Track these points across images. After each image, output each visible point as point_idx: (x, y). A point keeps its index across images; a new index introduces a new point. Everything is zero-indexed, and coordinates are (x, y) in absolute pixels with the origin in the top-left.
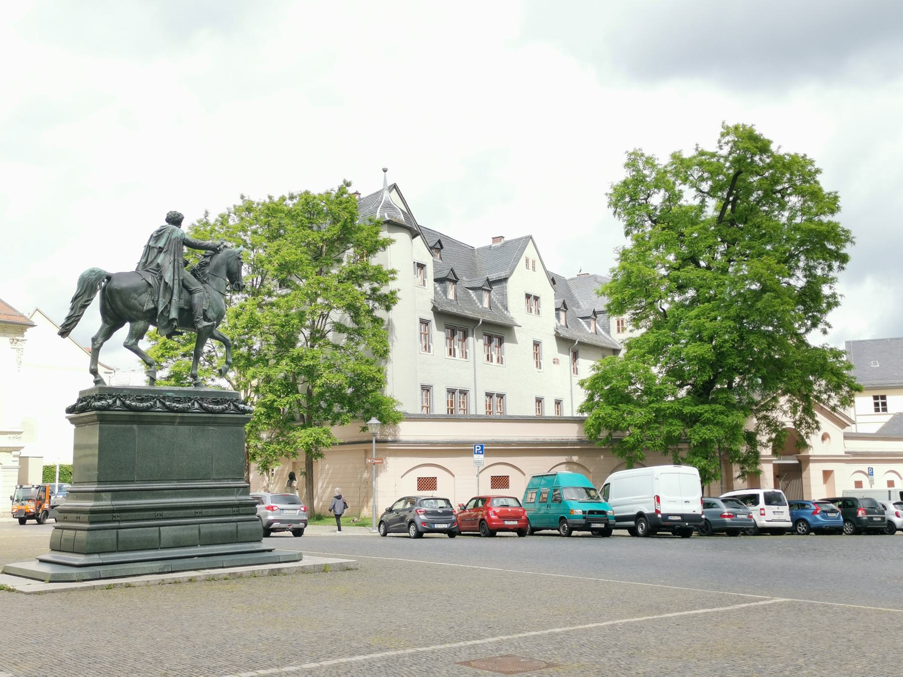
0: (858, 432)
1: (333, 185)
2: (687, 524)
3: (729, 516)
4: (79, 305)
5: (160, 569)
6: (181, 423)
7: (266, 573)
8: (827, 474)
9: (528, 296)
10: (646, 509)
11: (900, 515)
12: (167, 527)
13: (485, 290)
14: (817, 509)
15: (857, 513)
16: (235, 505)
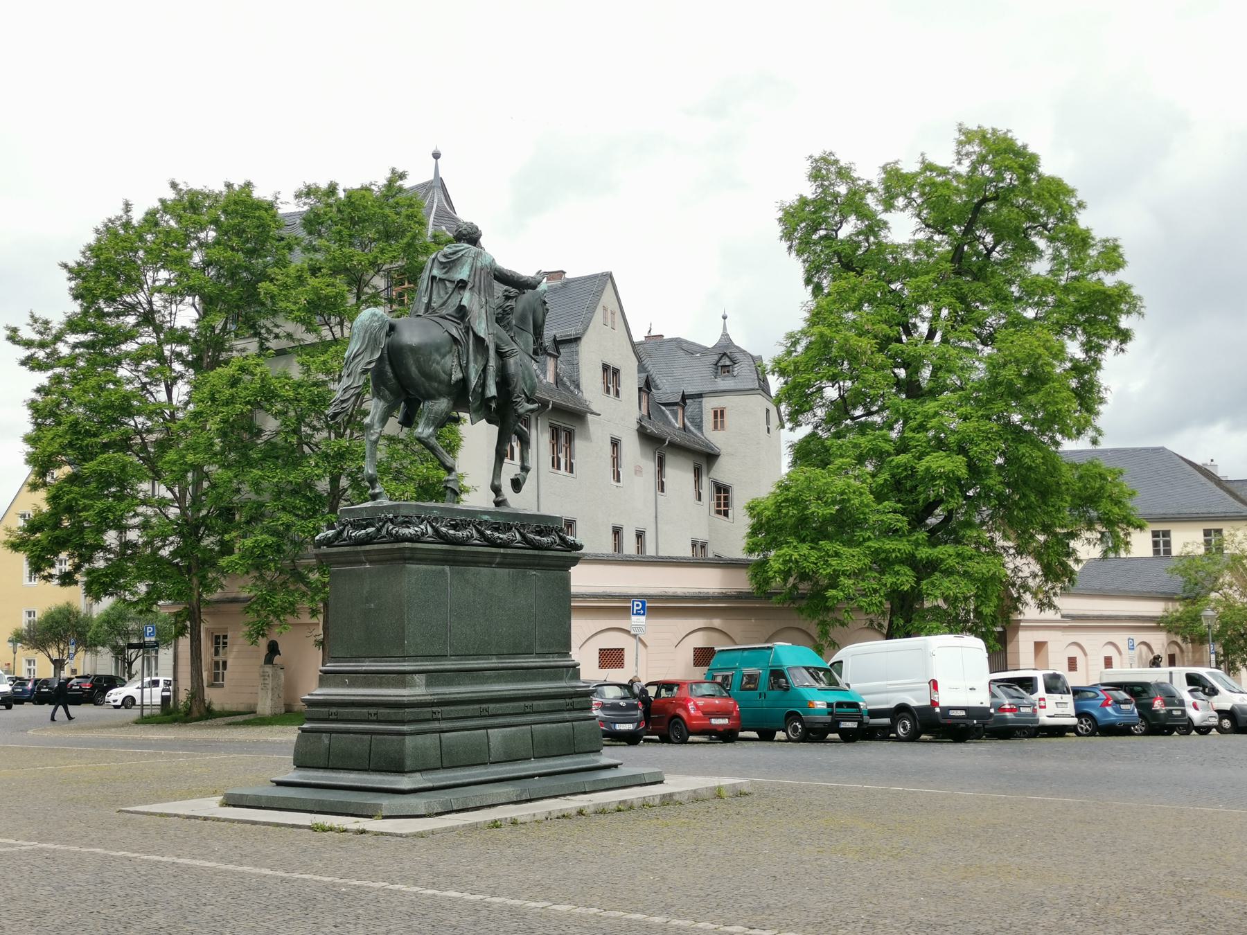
1: (379, 179)
2: (975, 722)
3: (1011, 710)
4: (359, 370)
6: (500, 565)
7: (657, 801)
8: (1039, 646)
9: (605, 368)
10: (914, 701)
11: (1199, 707)
12: (496, 730)
13: (550, 355)
14: (1108, 699)
15: (1152, 705)
16: (569, 695)
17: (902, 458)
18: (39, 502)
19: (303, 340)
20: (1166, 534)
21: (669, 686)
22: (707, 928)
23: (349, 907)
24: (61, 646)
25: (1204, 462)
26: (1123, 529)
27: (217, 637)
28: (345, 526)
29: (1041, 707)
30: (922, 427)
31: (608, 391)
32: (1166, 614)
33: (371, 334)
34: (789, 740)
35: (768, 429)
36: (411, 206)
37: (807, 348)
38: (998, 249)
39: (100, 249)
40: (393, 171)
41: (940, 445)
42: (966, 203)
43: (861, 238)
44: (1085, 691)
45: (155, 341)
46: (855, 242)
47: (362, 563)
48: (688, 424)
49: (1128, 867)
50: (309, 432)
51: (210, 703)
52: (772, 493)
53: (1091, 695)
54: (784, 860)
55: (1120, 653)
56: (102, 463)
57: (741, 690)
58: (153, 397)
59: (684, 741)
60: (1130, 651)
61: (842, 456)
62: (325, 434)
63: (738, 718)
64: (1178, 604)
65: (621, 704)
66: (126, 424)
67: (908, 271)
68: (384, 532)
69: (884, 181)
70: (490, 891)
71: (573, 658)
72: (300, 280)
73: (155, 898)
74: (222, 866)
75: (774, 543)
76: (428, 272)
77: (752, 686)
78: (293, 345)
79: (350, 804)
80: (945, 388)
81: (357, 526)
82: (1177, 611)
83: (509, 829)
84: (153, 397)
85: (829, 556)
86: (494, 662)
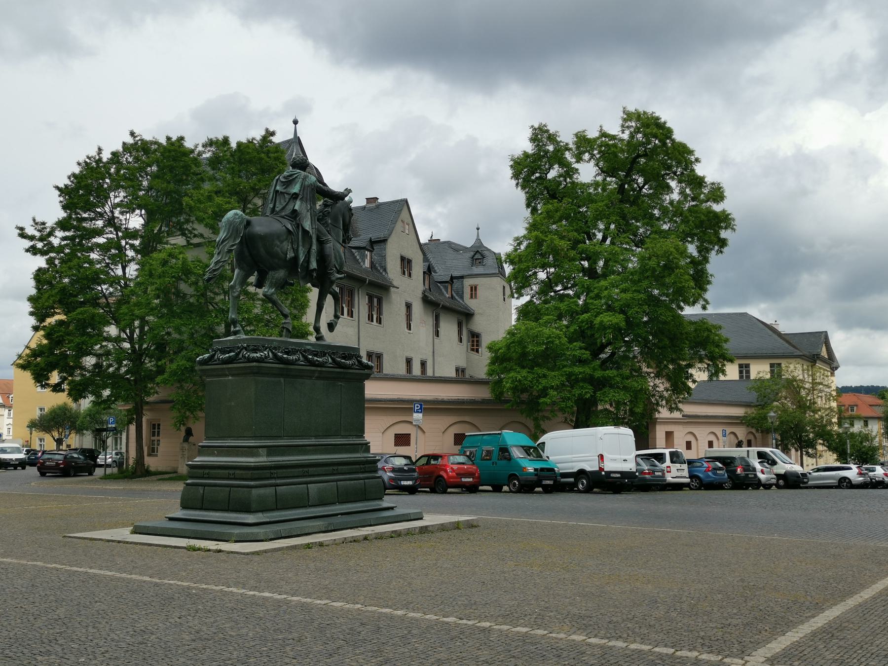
1: (257, 134)
3: (649, 474)
5: (325, 527)
6: (318, 378)
7: (417, 531)
8: (669, 435)
9: (403, 259)
12: (313, 485)
15: (736, 471)
17: (586, 316)
18: (38, 339)
19: (211, 238)
20: (747, 366)
21: (436, 457)
22: (432, 619)
23: (194, 604)
24: (61, 430)
25: (771, 323)
26: (721, 362)
27: (154, 425)
28: (216, 352)
29: (668, 472)
30: (598, 297)
31: (404, 273)
32: (746, 415)
33: (234, 227)
34: (511, 491)
35: (504, 298)
36: (277, 152)
37: (527, 247)
38: (646, 187)
39: (81, 178)
40: (267, 130)
41: (610, 308)
42: (627, 158)
43: (562, 179)
44: (694, 462)
45: (115, 236)
46: (558, 181)
47: (226, 375)
48: (455, 295)
49: (714, 576)
50: (212, 295)
51: (148, 466)
52: (504, 338)
53: (698, 464)
54: (492, 571)
55: (718, 439)
56: (79, 314)
57: (482, 460)
58: (114, 272)
59: (444, 492)
60: (724, 438)
61: (548, 315)
62: (222, 297)
63: (479, 477)
64: (753, 409)
65: (405, 468)
66: (96, 289)
67: (590, 200)
68: (240, 356)
69: (576, 143)
70: (292, 592)
71: (366, 439)
72: (210, 198)
73: (64, 597)
74: (118, 575)
75: (507, 370)
76: (273, 188)
77: (488, 458)
78: (204, 241)
79: (214, 532)
80: (613, 272)
81: (223, 352)
82: (753, 413)
83: (317, 550)
84: (114, 272)
85: (540, 378)
86: (313, 441)
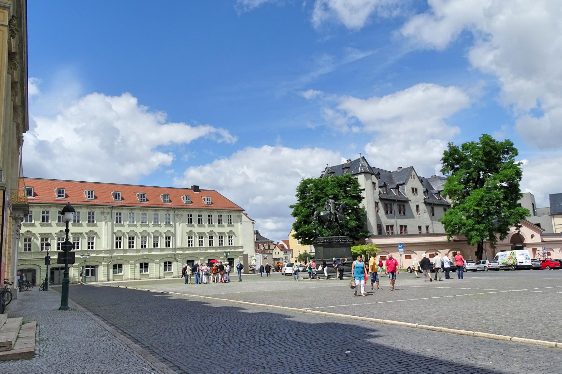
0: (557, 233)
9: (413, 189)
